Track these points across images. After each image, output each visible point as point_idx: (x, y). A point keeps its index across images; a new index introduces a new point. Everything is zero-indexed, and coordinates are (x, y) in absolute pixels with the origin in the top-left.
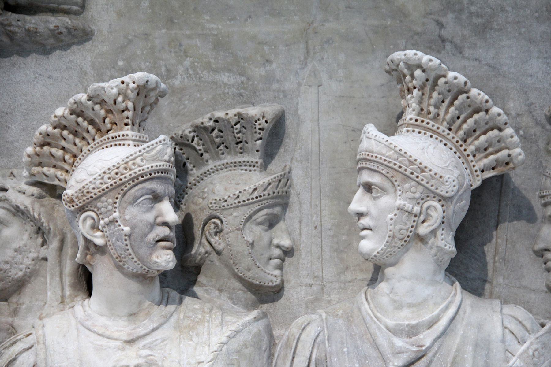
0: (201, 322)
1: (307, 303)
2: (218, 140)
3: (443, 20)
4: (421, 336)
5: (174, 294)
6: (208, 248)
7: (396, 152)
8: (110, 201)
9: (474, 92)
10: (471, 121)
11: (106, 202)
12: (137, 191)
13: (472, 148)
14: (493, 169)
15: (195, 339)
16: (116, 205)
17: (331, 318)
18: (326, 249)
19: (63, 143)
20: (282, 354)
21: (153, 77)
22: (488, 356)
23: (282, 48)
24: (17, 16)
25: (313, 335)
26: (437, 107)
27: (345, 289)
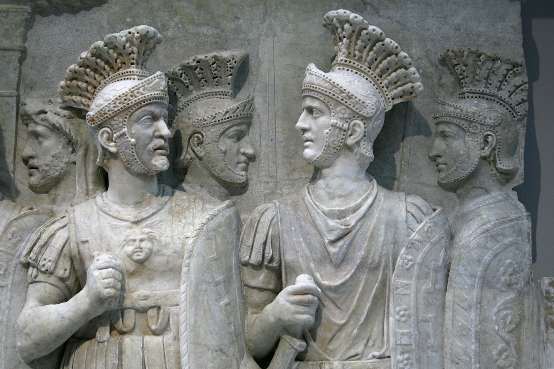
0: (188, 208)
2: (199, 76)
4: (348, 218)
6: (193, 155)
7: (331, 84)
9: (388, 40)
10: (385, 62)
11: (118, 120)
12: (140, 112)
13: (386, 81)
15: (183, 221)
16: (125, 123)
17: (282, 206)
18: (279, 156)
19: (87, 78)
21: (152, 29)
22: (395, 232)
26: (361, 51)
27: (293, 185)
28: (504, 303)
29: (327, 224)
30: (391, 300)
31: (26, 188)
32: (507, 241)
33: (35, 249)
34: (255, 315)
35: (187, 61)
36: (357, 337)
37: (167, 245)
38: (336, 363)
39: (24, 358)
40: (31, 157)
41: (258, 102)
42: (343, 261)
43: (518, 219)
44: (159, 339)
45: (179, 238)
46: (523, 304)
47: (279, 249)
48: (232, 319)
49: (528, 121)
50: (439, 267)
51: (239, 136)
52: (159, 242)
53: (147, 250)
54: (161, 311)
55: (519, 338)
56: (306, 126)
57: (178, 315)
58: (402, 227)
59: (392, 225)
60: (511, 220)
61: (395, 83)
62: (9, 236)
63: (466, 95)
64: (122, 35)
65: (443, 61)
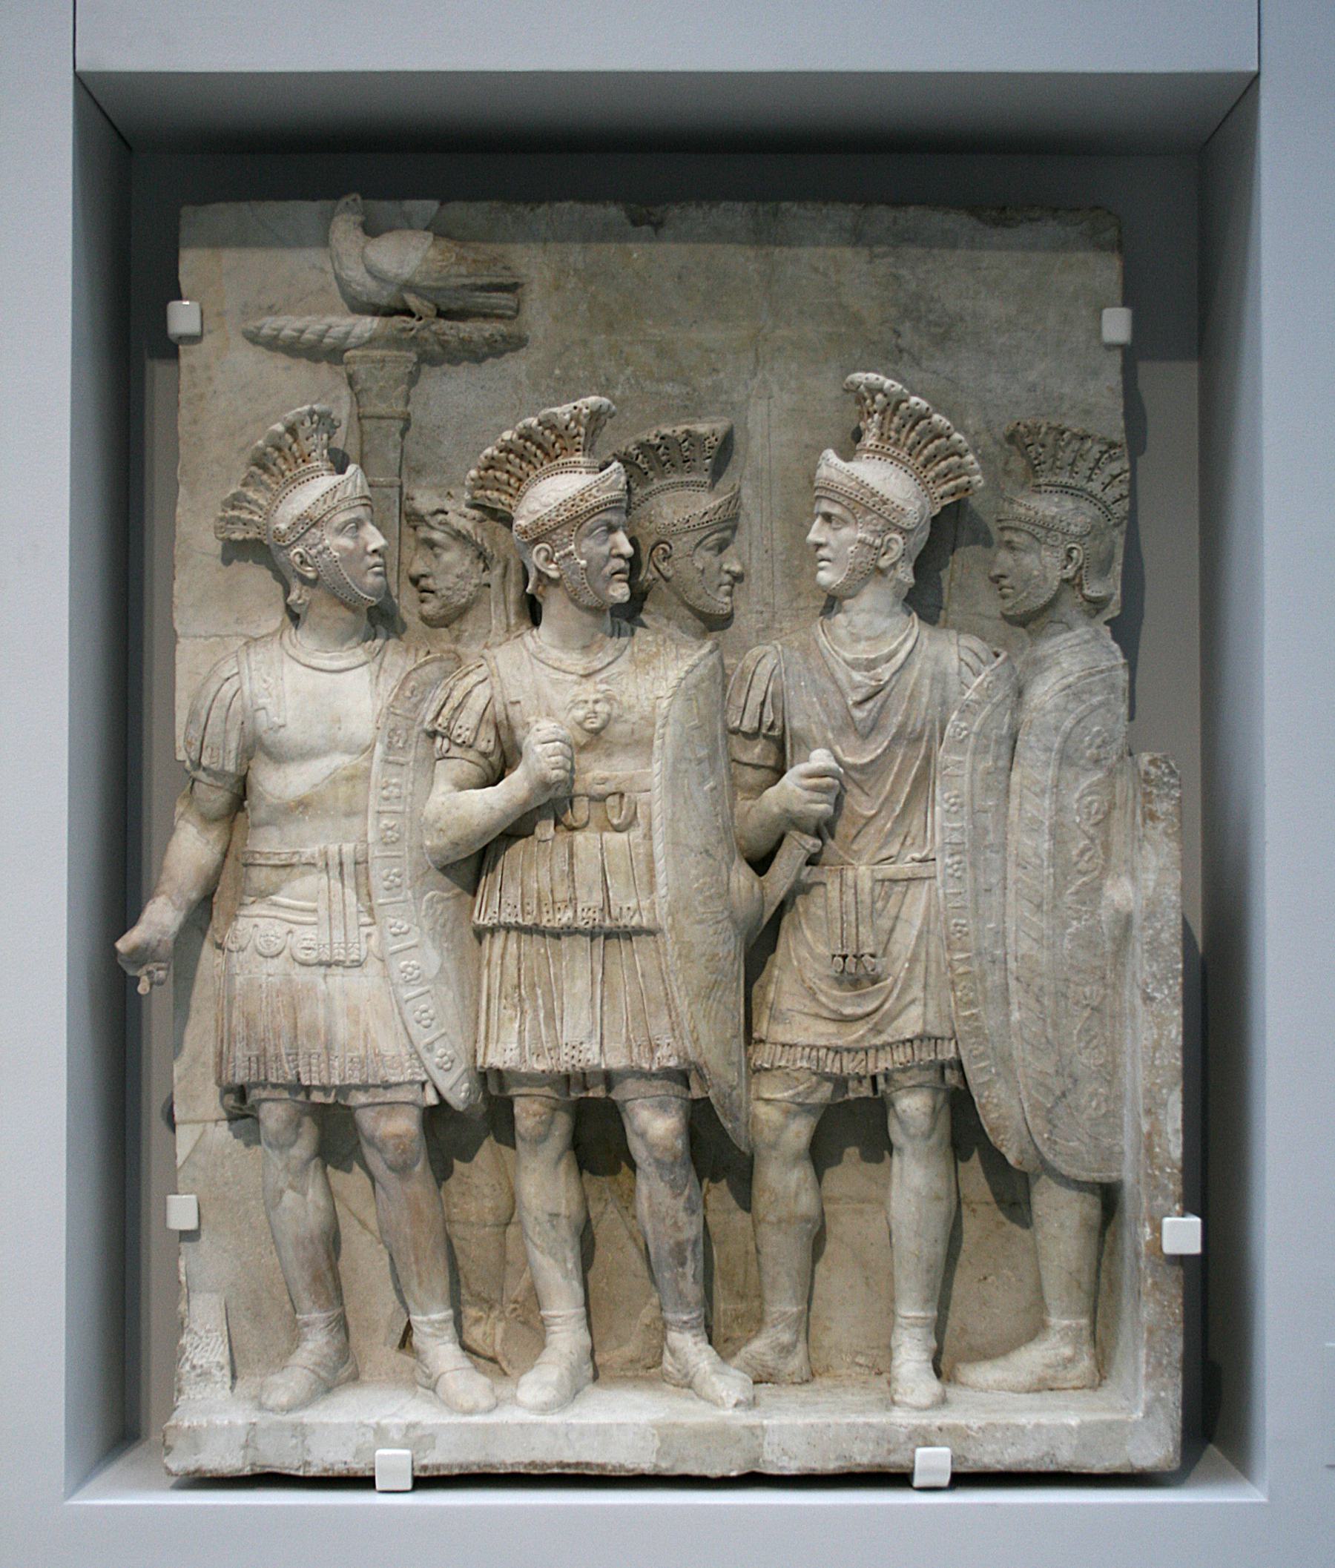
0: (657, 654)
1: (757, 632)
2: (664, 458)
3: (901, 328)
4: (879, 670)
5: (625, 624)
6: (657, 574)
8: (566, 533)
9: (936, 417)
10: (931, 447)
13: (932, 474)
14: (953, 495)
15: (652, 673)
17: (786, 651)
18: (778, 574)
19: (508, 467)
20: (737, 686)
21: (605, 401)
22: (944, 689)
23: (729, 357)
24: (450, 323)
25: (769, 667)
26: (898, 431)
27: (797, 616)
28: (1090, 786)
29: (850, 677)
30: (938, 783)
31: (417, 620)
32: (1095, 700)
33: (445, 711)
34: (749, 803)
35: (645, 437)
36: (892, 833)
37: (631, 708)
38: (862, 869)
39: (434, 862)
40: (423, 576)
41: (747, 493)
42: (872, 729)
43: (1112, 668)
44: (623, 836)
45: (647, 699)
46: (1114, 786)
47: (781, 711)
48: (719, 808)
49: (1129, 526)
50: (1001, 736)
51: (721, 547)
52: (620, 703)
53: (604, 716)
54: (626, 799)
55: (1107, 833)
56: (821, 540)
57: (649, 804)
58: (954, 687)
59: (939, 679)
60: (1102, 672)
61: (944, 475)
62: (408, 694)
63: (1043, 488)
64: (563, 411)
65: (1011, 438)
